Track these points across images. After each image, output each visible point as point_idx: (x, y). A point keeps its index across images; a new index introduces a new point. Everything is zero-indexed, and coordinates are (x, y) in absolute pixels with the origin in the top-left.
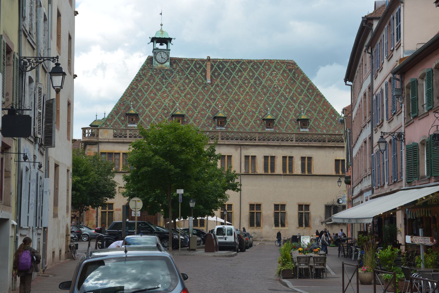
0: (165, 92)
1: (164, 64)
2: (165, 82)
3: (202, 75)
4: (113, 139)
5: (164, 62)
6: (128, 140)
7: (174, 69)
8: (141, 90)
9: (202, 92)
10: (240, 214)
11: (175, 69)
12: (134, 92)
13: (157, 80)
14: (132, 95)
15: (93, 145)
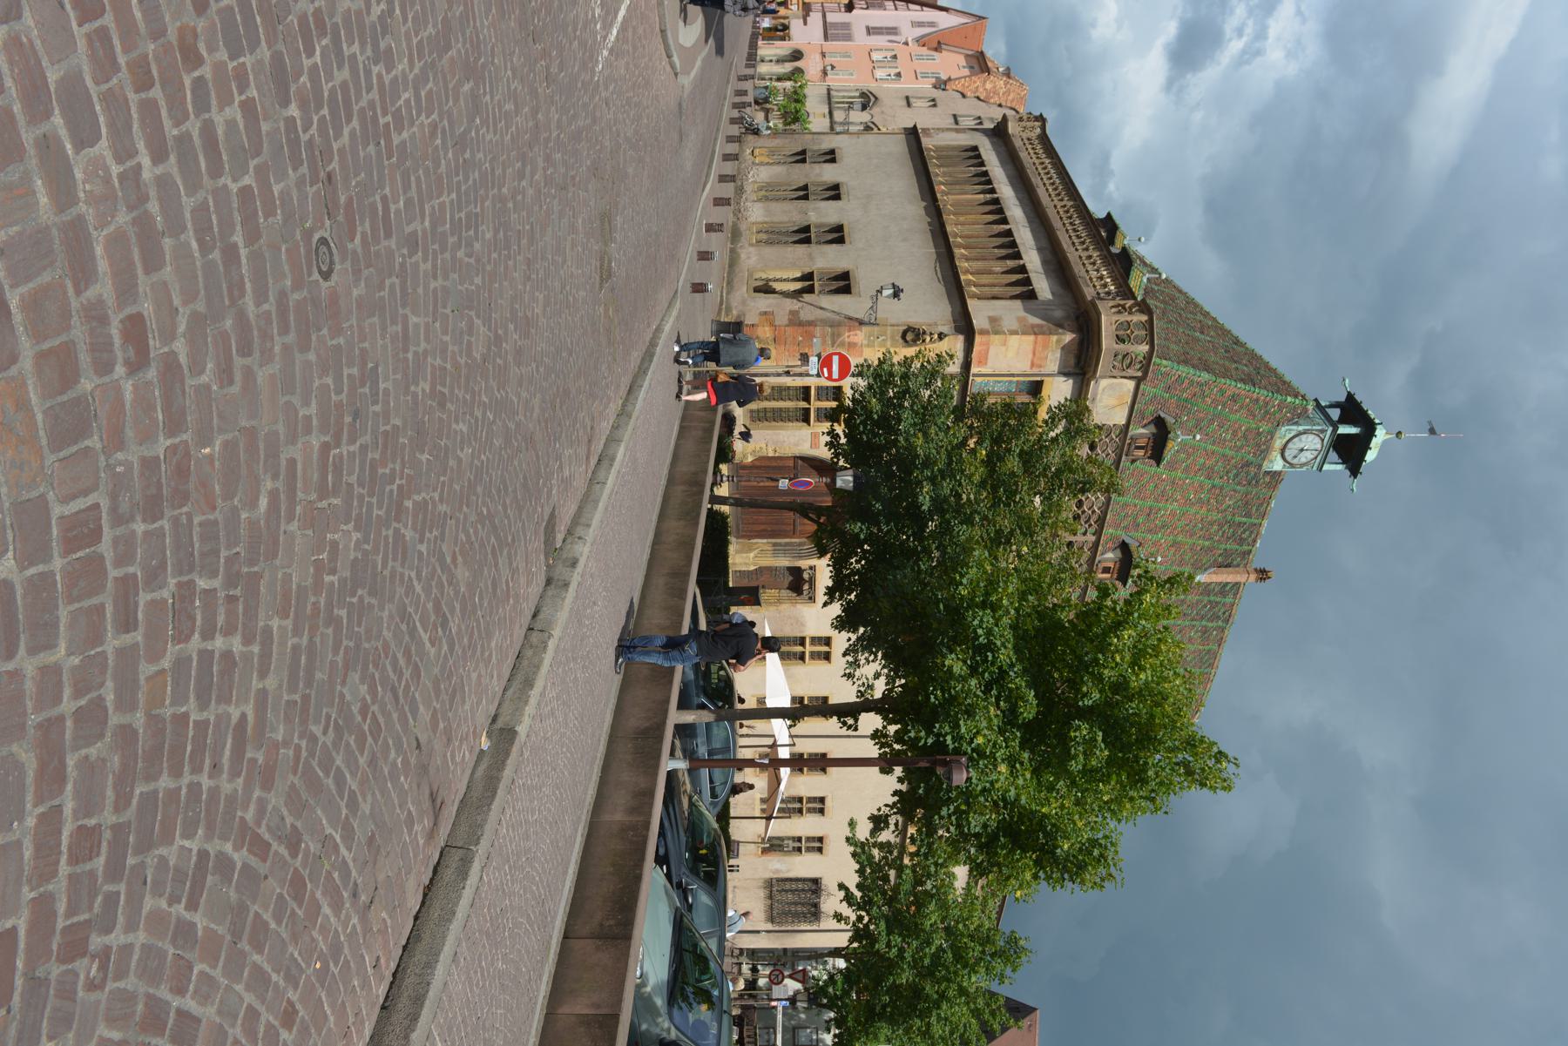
1: (1279, 457)
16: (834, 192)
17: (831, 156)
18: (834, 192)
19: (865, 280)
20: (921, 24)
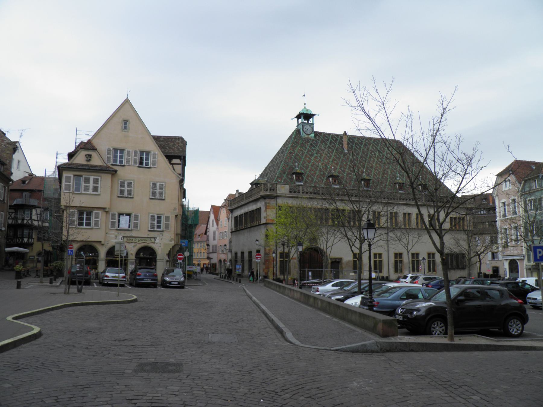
0: (316, 157)
1: (310, 135)
2: (315, 149)
3: (340, 146)
4: (289, 194)
5: (310, 133)
6: (116, 221)
7: (318, 140)
8: (298, 155)
9: (344, 160)
10: (388, 262)
11: (318, 140)
12: (293, 156)
13: (308, 147)
14: (292, 158)
15: (272, 198)
16: (243, 253)
17: (236, 254)
18: (243, 253)
19: (257, 248)
20: (213, 224)
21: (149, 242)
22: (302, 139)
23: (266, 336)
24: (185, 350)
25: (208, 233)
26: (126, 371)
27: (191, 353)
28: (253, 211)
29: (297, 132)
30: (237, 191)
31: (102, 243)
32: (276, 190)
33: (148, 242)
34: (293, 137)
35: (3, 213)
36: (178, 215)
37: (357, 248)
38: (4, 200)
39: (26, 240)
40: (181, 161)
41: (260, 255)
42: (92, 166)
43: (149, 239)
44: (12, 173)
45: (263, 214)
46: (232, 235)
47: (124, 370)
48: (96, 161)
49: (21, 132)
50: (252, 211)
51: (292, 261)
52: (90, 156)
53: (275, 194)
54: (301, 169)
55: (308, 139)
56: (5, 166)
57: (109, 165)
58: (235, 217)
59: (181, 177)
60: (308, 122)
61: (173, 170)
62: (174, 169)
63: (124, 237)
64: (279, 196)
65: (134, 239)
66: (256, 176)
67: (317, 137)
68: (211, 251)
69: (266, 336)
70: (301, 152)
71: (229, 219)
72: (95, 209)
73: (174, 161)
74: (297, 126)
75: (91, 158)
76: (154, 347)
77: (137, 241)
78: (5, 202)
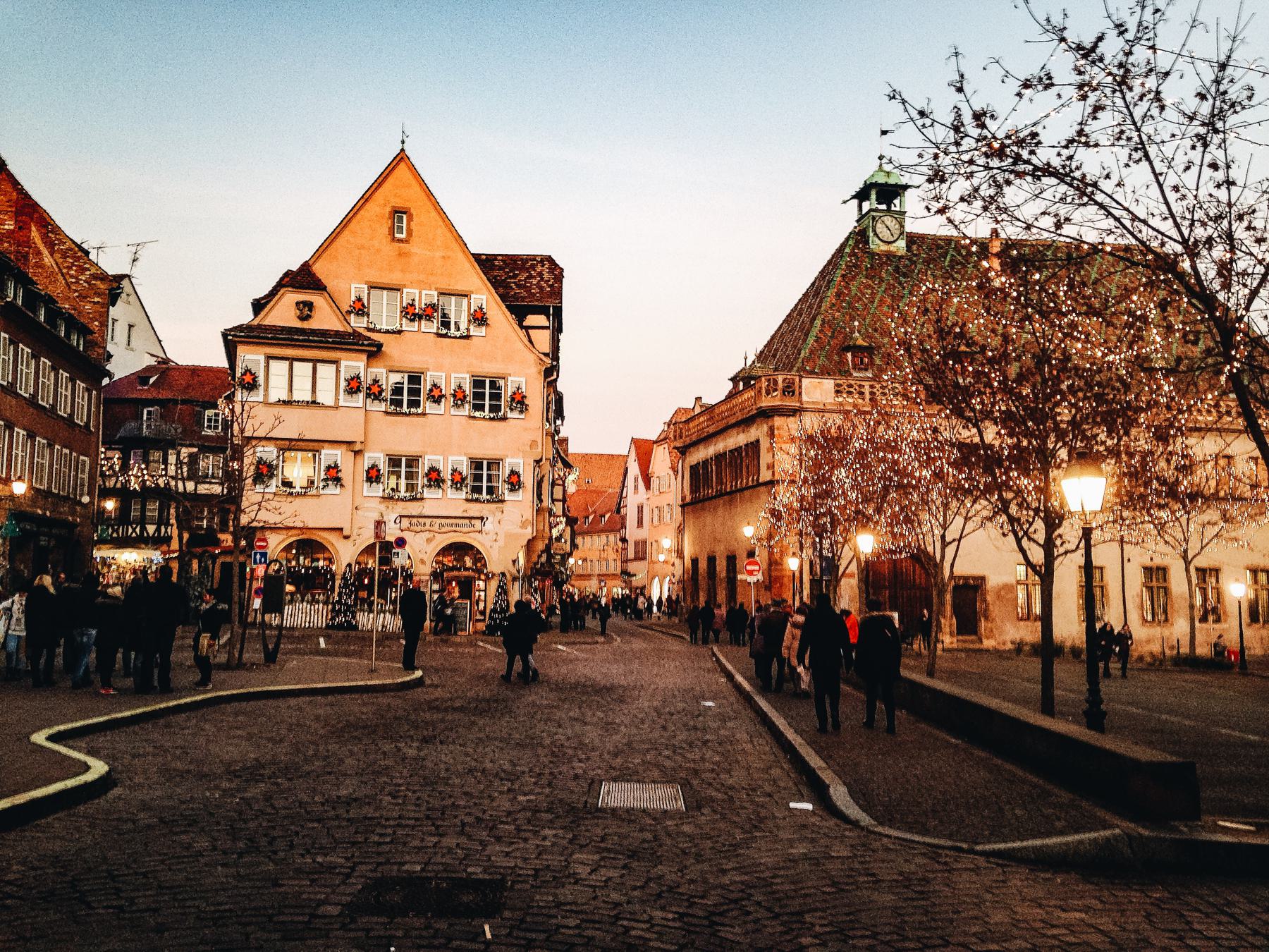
16: (712, 560)
17: (695, 562)
18: (712, 560)
20: (636, 488)
21: (468, 529)
22: (872, 254)
23: (769, 795)
24: (523, 834)
25: (623, 511)
26: (322, 910)
27: (538, 846)
28: (738, 449)
29: (860, 236)
30: (698, 399)
31: (346, 533)
32: (800, 393)
33: (465, 529)
34: (847, 250)
35: (86, 458)
36: (541, 460)
37: (1039, 545)
38: (87, 424)
39: (151, 529)
40: (548, 319)
41: (756, 563)
42: (314, 332)
43: (467, 521)
44: (110, 356)
45: (765, 458)
46: (683, 513)
47: (318, 906)
48: (325, 319)
49: (133, 249)
50: (736, 449)
51: (843, 581)
52: (310, 305)
53: (798, 405)
54: (867, 336)
55: (890, 256)
56: (89, 337)
57: (361, 331)
58: (691, 467)
59: (548, 361)
60: (889, 207)
61: (528, 343)
62: (530, 341)
63: (401, 516)
64: (805, 410)
65: (428, 521)
66: (746, 359)
67: (915, 247)
68: (631, 555)
69: (769, 795)
70: (869, 291)
71: (675, 471)
72: (326, 445)
73: (532, 320)
74: (858, 221)
75: (310, 310)
76: (433, 825)
77: (436, 528)
78: (92, 429)
